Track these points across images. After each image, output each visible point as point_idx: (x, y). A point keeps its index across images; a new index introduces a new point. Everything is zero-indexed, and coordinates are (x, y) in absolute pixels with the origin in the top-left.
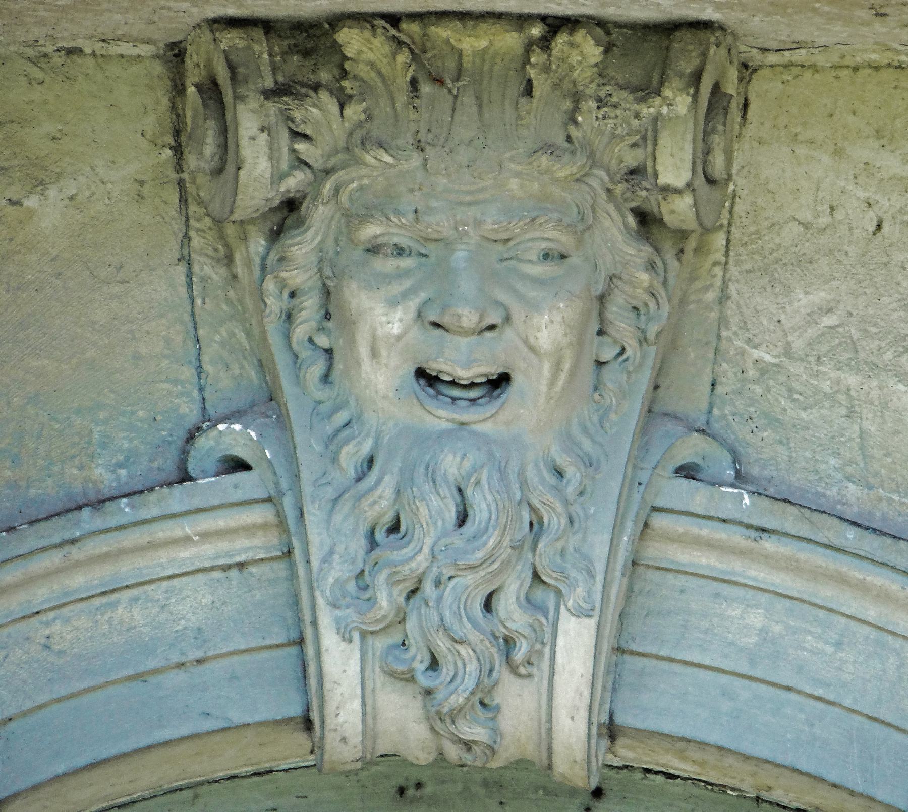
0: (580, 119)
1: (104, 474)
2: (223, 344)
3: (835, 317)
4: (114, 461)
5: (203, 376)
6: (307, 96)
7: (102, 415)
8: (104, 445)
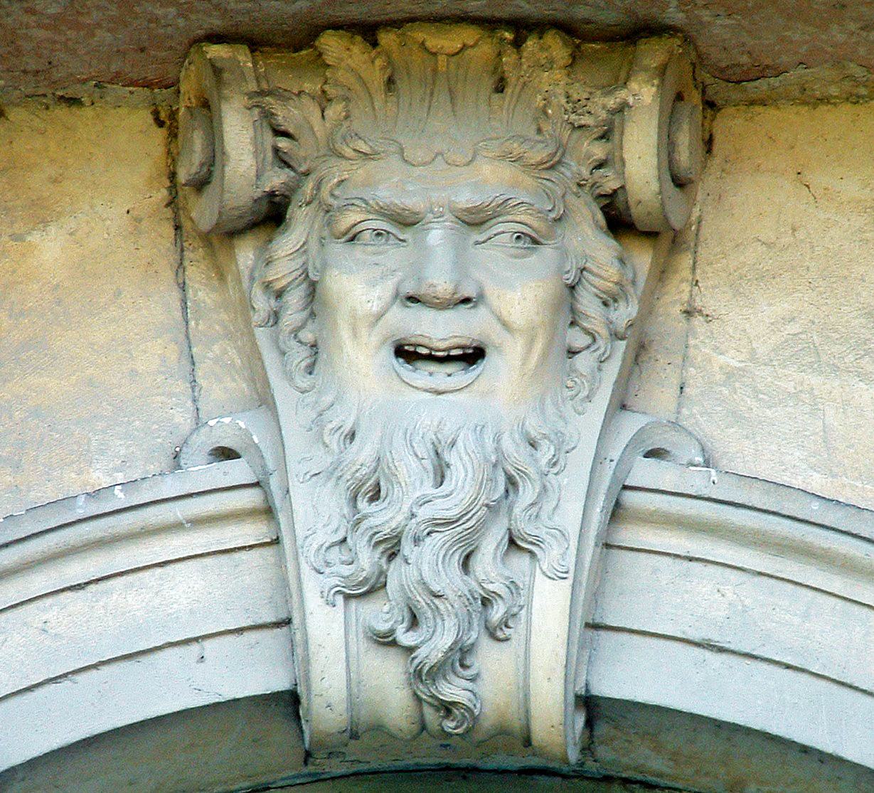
0: (550, 111)
1: (101, 477)
2: (216, 360)
3: (798, 326)
4: (111, 466)
5: (197, 389)
6: (289, 99)
7: (100, 425)
8: (102, 452)
